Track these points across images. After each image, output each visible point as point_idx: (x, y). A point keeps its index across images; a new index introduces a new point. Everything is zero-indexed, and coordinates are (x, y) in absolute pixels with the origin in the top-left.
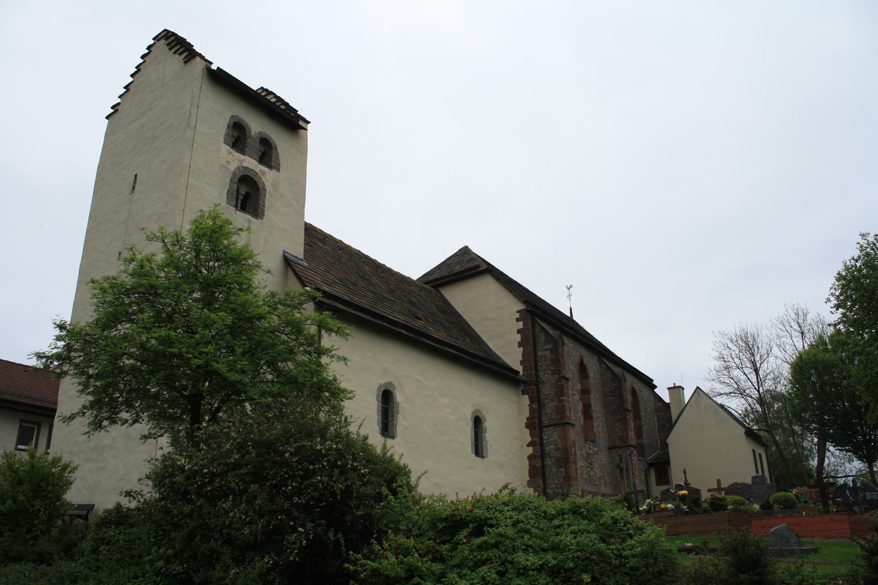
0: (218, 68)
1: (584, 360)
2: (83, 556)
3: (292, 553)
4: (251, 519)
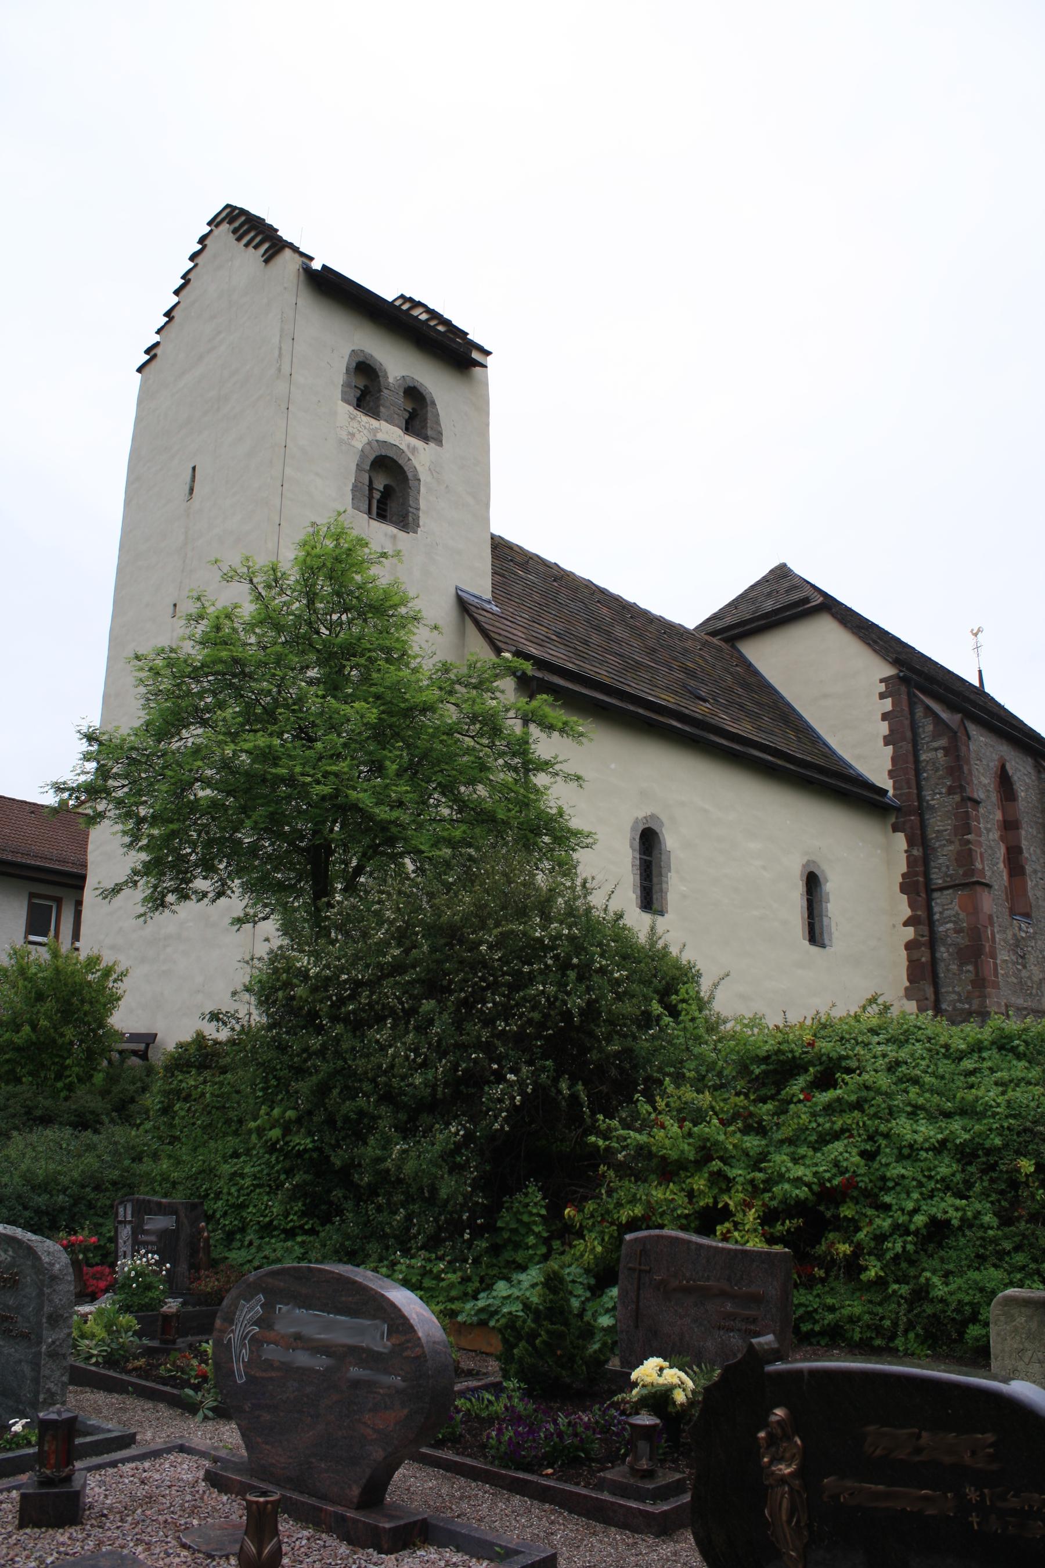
0: (324, 267)
1: (1008, 766)
2: (148, 1118)
3: (496, 1117)
4: (425, 1060)
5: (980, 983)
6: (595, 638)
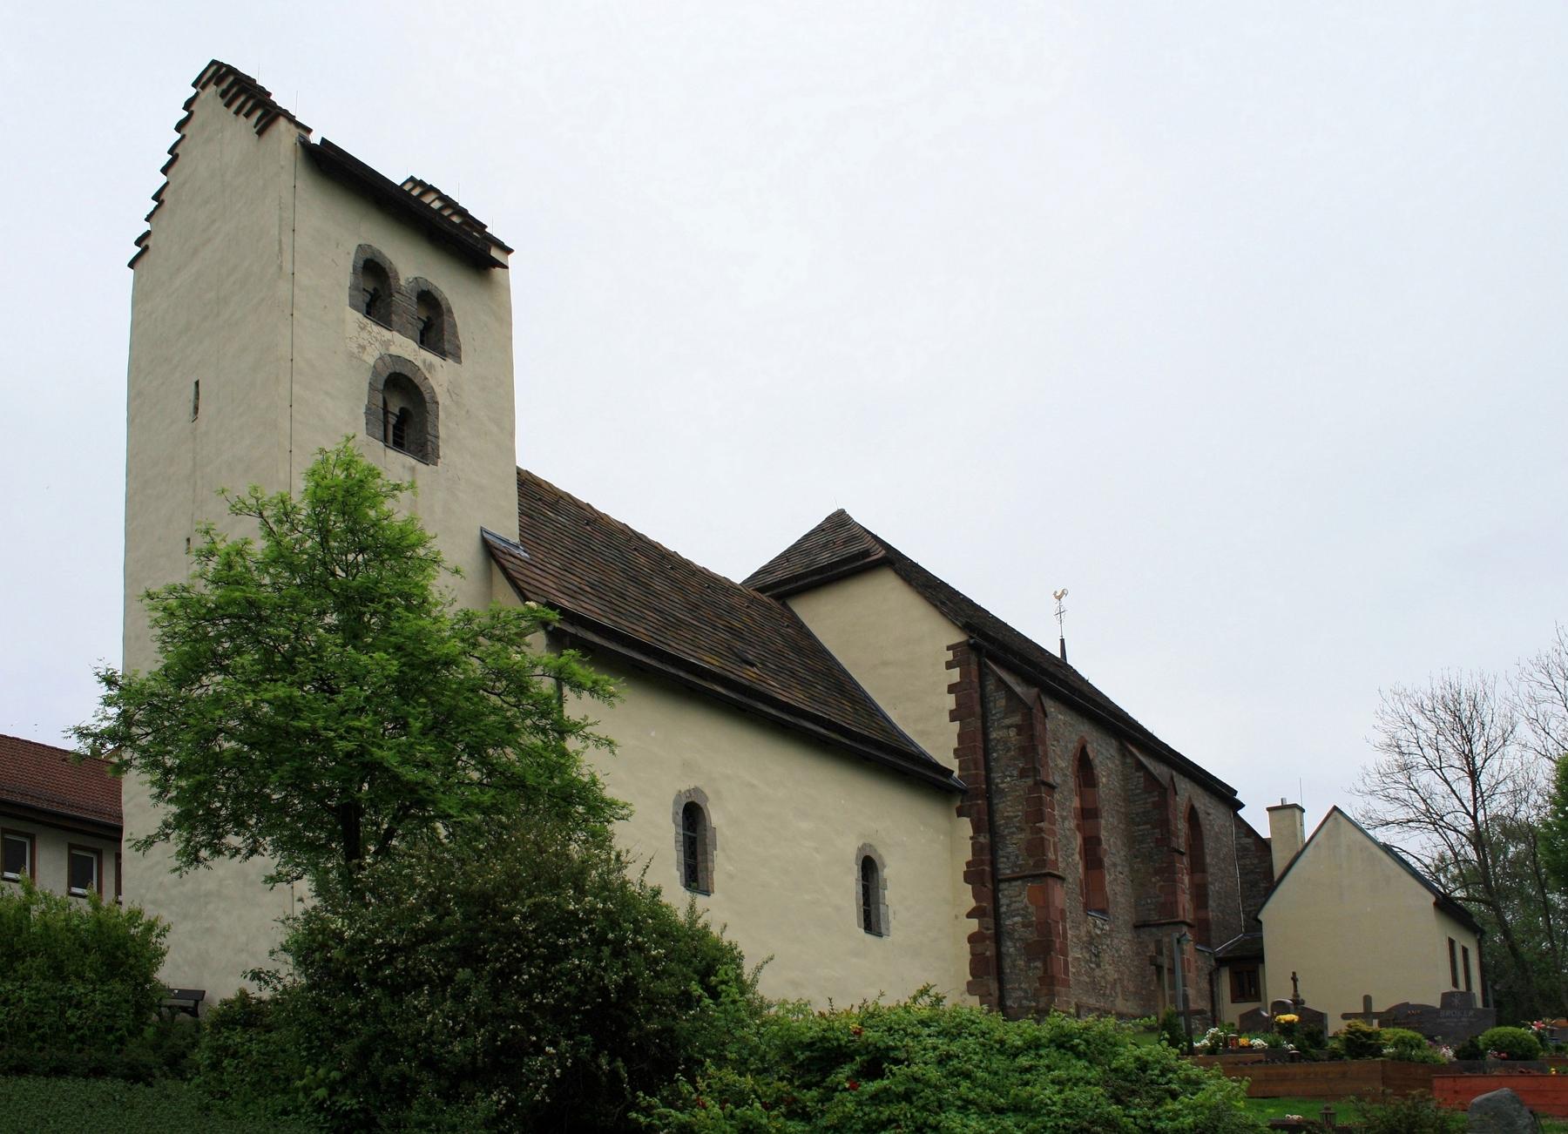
1: (1089, 749)
3: (537, 1088)
5: (1049, 981)
6: (632, 591)
